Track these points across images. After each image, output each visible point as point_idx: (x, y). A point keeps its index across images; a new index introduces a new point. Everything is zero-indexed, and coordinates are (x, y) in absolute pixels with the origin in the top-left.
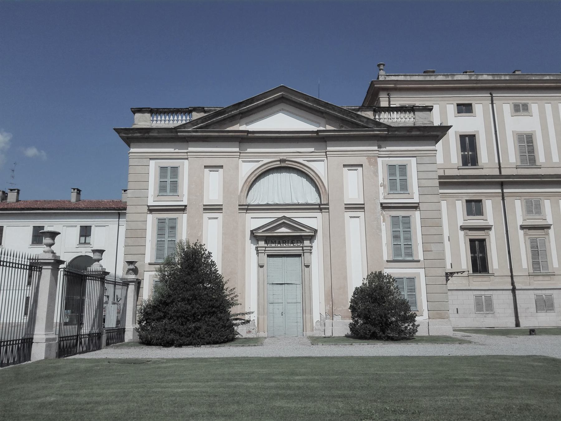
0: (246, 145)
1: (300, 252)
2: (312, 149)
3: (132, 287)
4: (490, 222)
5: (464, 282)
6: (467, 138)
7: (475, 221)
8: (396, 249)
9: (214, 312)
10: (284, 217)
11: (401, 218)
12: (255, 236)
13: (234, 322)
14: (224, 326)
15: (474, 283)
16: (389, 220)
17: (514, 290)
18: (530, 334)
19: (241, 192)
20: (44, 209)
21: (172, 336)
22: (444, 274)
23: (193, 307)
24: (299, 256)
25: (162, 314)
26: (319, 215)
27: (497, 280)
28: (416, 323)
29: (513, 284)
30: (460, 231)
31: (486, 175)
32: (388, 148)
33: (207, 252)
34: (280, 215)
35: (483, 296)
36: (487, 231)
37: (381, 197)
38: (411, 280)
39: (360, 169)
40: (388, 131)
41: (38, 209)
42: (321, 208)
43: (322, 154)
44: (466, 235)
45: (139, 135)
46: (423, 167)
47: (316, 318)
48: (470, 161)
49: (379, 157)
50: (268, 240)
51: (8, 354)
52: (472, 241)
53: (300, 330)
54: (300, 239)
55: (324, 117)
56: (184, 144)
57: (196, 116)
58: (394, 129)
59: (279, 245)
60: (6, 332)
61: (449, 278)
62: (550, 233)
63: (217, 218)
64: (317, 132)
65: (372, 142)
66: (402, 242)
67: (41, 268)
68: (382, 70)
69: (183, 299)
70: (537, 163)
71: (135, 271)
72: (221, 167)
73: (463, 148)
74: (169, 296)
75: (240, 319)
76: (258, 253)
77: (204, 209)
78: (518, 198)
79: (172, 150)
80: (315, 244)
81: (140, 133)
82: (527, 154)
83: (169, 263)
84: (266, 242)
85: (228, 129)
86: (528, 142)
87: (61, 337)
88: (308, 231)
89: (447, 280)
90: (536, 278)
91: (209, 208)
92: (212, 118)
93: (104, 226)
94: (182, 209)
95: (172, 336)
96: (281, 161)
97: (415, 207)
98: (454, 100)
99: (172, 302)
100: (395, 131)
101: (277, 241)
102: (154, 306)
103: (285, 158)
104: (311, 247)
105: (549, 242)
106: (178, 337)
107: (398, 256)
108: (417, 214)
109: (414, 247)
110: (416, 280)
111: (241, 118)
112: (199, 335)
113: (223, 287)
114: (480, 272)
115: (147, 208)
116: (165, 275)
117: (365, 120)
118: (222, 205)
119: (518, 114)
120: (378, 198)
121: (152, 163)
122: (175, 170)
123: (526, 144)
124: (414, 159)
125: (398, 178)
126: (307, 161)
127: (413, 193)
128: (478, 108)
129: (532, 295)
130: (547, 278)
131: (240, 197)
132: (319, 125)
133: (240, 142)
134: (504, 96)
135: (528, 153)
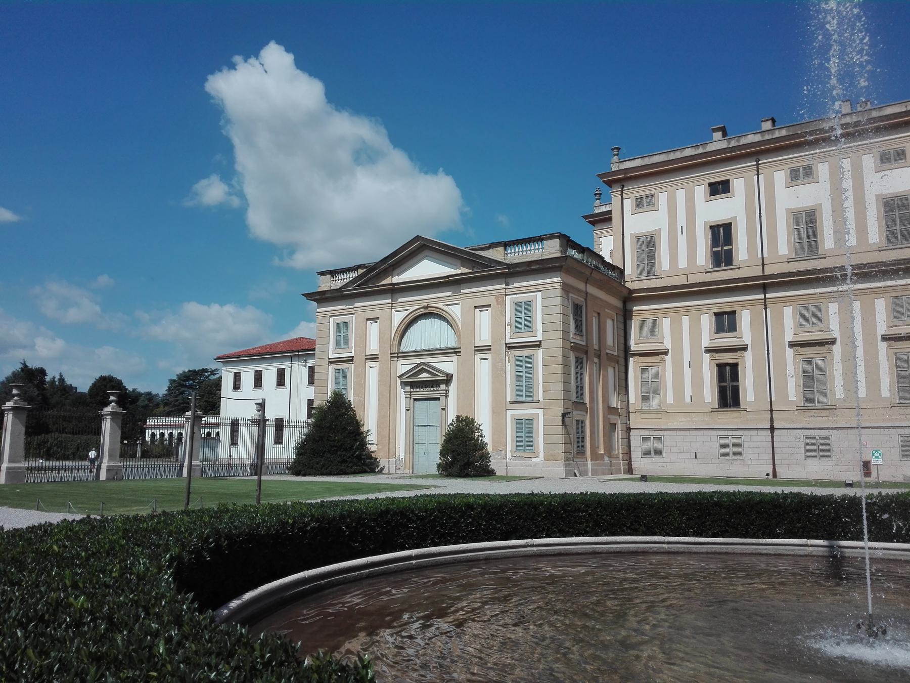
0: (398, 295)
2: (450, 293)
6: (721, 229)
10: (422, 363)
11: (524, 357)
15: (719, 420)
16: (513, 360)
22: (560, 415)
26: (454, 358)
27: (750, 416)
29: (772, 420)
30: (704, 354)
31: (774, 274)
32: (516, 285)
34: (419, 361)
35: (730, 437)
36: (741, 352)
37: (508, 336)
38: (530, 421)
40: (509, 268)
44: (711, 359)
45: (318, 297)
46: (548, 302)
48: (723, 260)
50: (413, 385)
57: (361, 271)
58: (514, 266)
59: (422, 390)
62: (834, 350)
64: (448, 276)
66: (524, 382)
70: (820, 252)
73: (715, 241)
78: (788, 304)
79: (344, 307)
85: (381, 284)
88: (441, 375)
96: (426, 307)
97: (538, 345)
98: (704, 180)
100: (516, 267)
107: (520, 397)
110: (535, 421)
111: (393, 270)
114: (730, 407)
117: (488, 260)
119: (796, 182)
123: (804, 226)
124: (539, 294)
125: (523, 315)
128: (738, 185)
132: (455, 267)
133: (392, 293)
134: (776, 161)
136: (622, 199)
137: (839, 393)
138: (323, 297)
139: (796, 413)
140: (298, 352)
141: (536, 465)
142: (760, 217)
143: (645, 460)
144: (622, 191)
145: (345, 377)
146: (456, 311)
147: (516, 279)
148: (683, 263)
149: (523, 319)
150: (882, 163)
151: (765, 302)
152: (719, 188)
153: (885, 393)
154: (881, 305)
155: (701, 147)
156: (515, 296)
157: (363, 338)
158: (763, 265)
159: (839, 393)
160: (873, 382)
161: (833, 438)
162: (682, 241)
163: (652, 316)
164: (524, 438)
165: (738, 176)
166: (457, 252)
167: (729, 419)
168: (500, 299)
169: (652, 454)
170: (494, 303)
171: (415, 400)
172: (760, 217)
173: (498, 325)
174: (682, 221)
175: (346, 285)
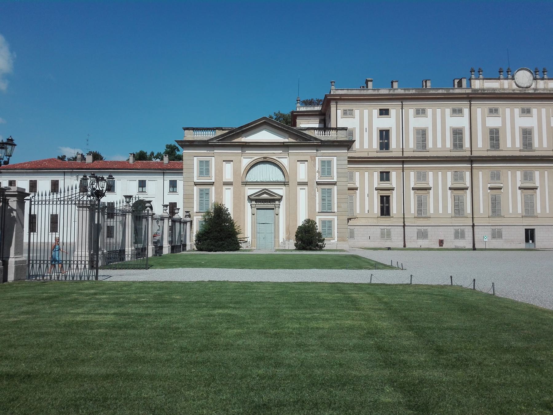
0: (244, 149)
1: (274, 207)
2: (281, 152)
3: (188, 224)
4: (394, 185)
5: (375, 221)
6: (384, 132)
7: (385, 185)
8: (323, 206)
9: (230, 237)
12: (250, 199)
13: (239, 242)
14: (235, 244)
15: (381, 222)
16: (320, 191)
17: (404, 226)
18: (388, 250)
19: (243, 175)
20: (114, 169)
21: (212, 247)
23: (220, 235)
24: (273, 209)
25: (206, 238)
26: (284, 187)
27: (395, 220)
28: (325, 243)
29: (404, 222)
30: (375, 190)
32: (322, 151)
33: (226, 208)
37: (317, 178)
38: (330, 222)
39: (306, 163)
41: (111, 169)
42: (285, 184)
43: (286, 154)
44: (378, 193)
46: (340, 162)
47: (281, 240)
49: (316, 156)
50: (257, 201)
51: (35, 269)
52: (382, 197)
53: (273, 246)
54: (274, 200)
55: (287, 133)
56: (212, 148)
59: (263, 204)
60: (533, 226)
61: (349, 221)
63: (230, 189)
64: (283, 143)
65: (313, 148)
66: (326, 202)
67: (164, 219)
68: (333, 85)
69: (216, 231)
70: (464, 148)
71: (189, 216)
72: (232, 161)
73: (381, 137)
74: (209, 229)
75: (242, 241)
76: (251, 208)
77: (223, 184)
79: (206, 151)
80: (281, 203)
81: (189, 143)
82: (421, 143)
83: (208, 213)
84: (256, 202)
86: (422, 135)
87: (108, 252)
89: (348, 222)
90: (418, 219)
91: (226, 184)
92: (227, 135)
93: (155, 181)
94: (212, 184)
95: (212, 247)
97: (334, 184)
98: (378, 107)
99: (211, 232)
100: (325, 143)
101: (262, 202)
102: (202, 234)
103: (266, 156)
104: (280, 205)
105: (429, 198)
106: (215, 248)
108: (335, 187)
109: (332, 205)
110: (332, 222)
111: (243, 133)
112: (224, 247)
113: (234, 225)
114: (385, 216)
115: (194, 183)
116: (206, 219)
117: (309, 136)
118: (233, 182)
119: (419, 116)
120: (315, 179)
121: (195, 158)
122: (207, 162)
125: (326, 168)
126: (278, 158)
127: (334, 176)
128: (393, 112)
129: (415, 229)
130: (426, 219)
131: (242, 178)
135: (422, 142)
136: (337, 109)
137: (432, 211)
138: (192, 144)
139: (451, 219)
140: (73, 170)
141: (333, 243)
142: (402, 128)
143: (493, 240)
144: (337, 105)
145: (208, 194)
146: (284, 162)
147: (322, 148)
148: (366, 146)
149: (326, 169)
150: (453, 113)
151: (403, 169)
152: (384, 112)
153: (413, 212)
154: (449, 174)
155: (376, 90)
156: (321, 157)
157: (220, 172)
158: (403, 152)
159: (432, 211)
160: (445, 207)
161: (429, 230)
162: (366, 135)
163: (350, 171)
164: (327, 230)
165: (393, 108)
166: (290, 130)
167: (385, 221)
168: (313, 158)
169: (460, 238)
170: (309, 159)
171: (257, 209)
172: (402, 128)
173: (311, 171)
174: (366, 125)
175: (212, 139)
